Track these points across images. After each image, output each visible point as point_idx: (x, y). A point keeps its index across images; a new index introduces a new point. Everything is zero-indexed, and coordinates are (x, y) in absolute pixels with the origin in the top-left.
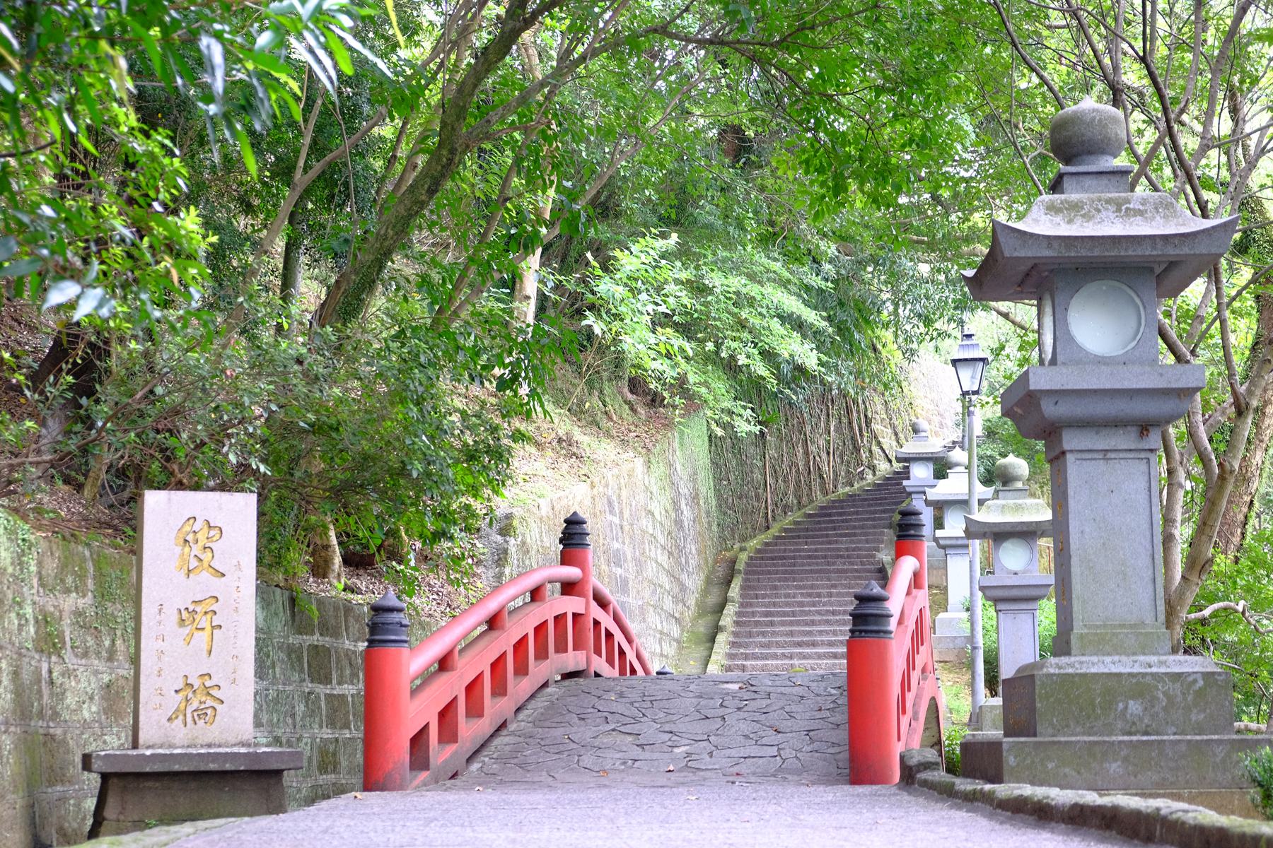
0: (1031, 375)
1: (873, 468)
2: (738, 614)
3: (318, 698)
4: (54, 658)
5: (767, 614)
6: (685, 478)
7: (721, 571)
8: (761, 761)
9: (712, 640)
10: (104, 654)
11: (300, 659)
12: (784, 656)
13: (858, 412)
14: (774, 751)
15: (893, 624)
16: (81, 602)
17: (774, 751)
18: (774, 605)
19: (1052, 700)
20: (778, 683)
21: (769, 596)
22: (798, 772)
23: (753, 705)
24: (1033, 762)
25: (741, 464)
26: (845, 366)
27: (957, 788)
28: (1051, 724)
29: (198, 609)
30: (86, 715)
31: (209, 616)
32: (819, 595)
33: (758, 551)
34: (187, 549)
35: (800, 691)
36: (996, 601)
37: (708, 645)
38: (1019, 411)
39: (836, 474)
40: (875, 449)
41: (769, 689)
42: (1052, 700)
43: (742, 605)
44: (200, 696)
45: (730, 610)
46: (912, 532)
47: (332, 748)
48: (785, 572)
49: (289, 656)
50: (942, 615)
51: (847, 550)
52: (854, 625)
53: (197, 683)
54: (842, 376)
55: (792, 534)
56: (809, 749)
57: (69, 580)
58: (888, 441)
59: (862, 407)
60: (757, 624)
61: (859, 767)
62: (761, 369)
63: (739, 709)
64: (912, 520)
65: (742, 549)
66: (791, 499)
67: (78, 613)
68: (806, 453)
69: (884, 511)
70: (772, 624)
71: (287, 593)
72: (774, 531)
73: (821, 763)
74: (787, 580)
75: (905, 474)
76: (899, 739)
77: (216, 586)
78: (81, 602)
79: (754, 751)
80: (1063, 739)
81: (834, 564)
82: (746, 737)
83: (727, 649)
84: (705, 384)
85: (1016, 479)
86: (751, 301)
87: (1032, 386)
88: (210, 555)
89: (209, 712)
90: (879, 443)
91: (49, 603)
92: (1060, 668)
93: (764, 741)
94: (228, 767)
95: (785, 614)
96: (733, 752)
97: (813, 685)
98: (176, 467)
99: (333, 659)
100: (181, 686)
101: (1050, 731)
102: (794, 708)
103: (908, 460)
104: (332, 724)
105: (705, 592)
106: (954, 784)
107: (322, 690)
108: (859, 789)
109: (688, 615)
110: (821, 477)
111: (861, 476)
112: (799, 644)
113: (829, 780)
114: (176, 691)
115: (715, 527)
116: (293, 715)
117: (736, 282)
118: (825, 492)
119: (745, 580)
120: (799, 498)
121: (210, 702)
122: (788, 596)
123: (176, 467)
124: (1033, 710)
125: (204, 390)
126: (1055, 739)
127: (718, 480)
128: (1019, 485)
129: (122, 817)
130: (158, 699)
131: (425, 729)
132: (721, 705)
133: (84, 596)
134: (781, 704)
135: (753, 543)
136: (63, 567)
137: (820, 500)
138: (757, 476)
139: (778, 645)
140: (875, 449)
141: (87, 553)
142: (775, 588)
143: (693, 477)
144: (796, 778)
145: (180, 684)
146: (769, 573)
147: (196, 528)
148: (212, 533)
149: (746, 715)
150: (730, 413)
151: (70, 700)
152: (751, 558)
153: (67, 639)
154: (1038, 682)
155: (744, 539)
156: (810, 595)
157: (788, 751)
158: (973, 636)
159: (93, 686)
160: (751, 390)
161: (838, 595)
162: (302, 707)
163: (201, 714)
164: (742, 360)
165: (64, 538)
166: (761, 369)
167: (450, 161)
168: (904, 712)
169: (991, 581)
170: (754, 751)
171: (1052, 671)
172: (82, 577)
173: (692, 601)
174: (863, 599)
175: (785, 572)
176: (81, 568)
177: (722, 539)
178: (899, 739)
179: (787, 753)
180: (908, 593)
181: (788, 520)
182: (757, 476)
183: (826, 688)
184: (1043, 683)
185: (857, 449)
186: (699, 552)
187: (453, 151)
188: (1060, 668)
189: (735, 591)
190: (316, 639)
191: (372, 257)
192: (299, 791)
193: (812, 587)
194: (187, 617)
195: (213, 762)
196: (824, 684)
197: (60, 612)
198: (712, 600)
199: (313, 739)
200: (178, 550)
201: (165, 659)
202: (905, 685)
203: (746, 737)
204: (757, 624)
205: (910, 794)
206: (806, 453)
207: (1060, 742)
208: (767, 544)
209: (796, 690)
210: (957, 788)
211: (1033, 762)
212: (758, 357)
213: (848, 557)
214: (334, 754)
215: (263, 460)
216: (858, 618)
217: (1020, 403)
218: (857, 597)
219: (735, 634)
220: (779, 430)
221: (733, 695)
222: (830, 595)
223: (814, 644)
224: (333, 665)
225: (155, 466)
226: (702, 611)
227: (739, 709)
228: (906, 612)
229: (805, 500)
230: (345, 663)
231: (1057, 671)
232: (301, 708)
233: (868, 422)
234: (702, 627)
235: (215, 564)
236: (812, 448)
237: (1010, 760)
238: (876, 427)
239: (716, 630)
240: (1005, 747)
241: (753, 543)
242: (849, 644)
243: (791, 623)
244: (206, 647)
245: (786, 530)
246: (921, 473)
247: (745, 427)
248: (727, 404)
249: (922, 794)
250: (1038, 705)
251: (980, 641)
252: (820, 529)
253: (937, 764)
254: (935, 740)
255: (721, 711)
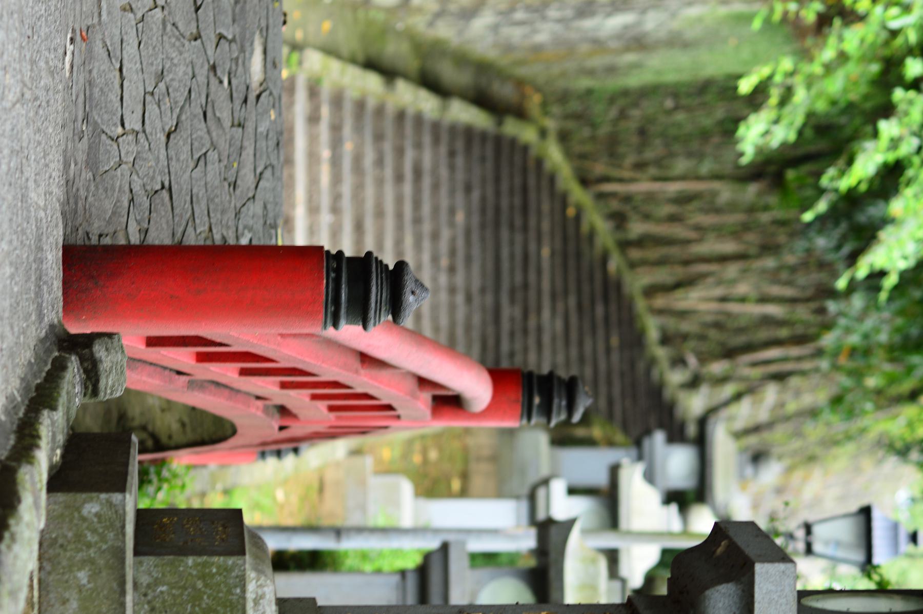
0: (781, 566)
1: (694, 383)
2: (419, 119)
5: (418, 173)
6: (675, 25)
7: (504, 91)
8: (114, 98)
9: (371, 64)
12: (336, 198)
13: (799, 359)
14: (133, 123)
15: (349, 333)
17: (133, 123)
18: (436, 187)
19: (200, 585)
20: (262, 144)
21: (452, 179)
22: (92, 162)
23: (220, 94)
24: (89, 546)
26: (881, 326)
27: (45, 412)
28: (157, 582)
32: (452, 270)
33: (539, 162)
35: (247, 179)
36: (423, 571)
37: (361, 57)
38: (720, 550)
39: (683, 314)
40: (729, 390)
41: (250, 126)
42: (200, 585)
43: (436, 127)
45: (426, 103)
46: (537, 400)
48: (497, 210)
51: (539, 329)
52: (350, 260)
54: (861, 318)
55: (572, 237)
56: (137, 188)
58: (744, 412)
59: (807, 365)
60: (400, 152)
61: (91, 265)
62: (866, 164)
63: (213, 68)
65: (543, 133)
66: (637, 228)
68: (723, 259)
69: (610, 403)
70: (399, 178)
72: (578, 195)
73: (108, 206)
74: (483, 211)
75: (676, 435)
76: (153, 342)
79: (133, 90)
80: (129, 598)
81: (512, 301)
82: (161, 75)
83: (352, 94)
84: (843, 57)
87: (760, 568)
90: (738, 397)
92: (256, 602)
93: (152, 108)
95: (417, 204)
96: (131, 49)
97: (256, 208)
101: (145, 580)
102: (214, 168)
103: (701, 443)
105: (461, 59)
106: (53, 408)
108: (53, 259)
109: (418, 23)
110: (678, 285)
111: (679, 362)
113: (72, 210)
115: (585, 83)
118: (651, 291)
119: (484, 136)
120: (641, 242)
122: (452, 211)
124: (183, 551)
126: (129, 586)
127: (675, 91)
131: (882, 274)
132: (221, 37)
134: (223, 145)
135: (554, 155)
137: (636, 282)
139: (359, 187)
140: (729, 390)
142: (468, 189)
143: (676, 41)
144: (81, 157)
146: (497, 179)
149: (201, 79)
150: (784, 100)
152: (525, 148)
154: (230, 561)
155: (564, 137)
156: (453, 253)
157: (133, 148)
158: (360, 530)
160: (830, 138)
161: (452, 308)
166: (866, 164)
168: (202, 358)
169: (458, 565)
170: (133, 90)
171: (251, 587)
173: (445, 31)
174: (397, 277)
175: (497, 210)
177: (564, 97)
178: (153, 342)
179: (128, 147)
180: (423, 382)
181: (598, 222)
182: (681, 165)
183: (250, 229)
184: (229, 570)
185: (730, 353)
186: (537, 49)
188: (256, 602)
189: (463, 113)
193: (468, 259)
196: (259, 226)
198: (448, 73)
202: (252, 363)
203: (161, 75)
204: (400, 152)
205: (42, 341)
206: (723, 259)
207: (123, 593)
208: (552, 179)
209: (247, 179)
210: (45, 412)
211: (89, 546)
212: (891, 157)
213: (525, 331)
216: (362, 268)
217: (734, 550)
218: (401, 266)
219: (380, 111)
220: (766, 208)
221: (241, 60)
222: (452, 290)
226: (429, 50)
227: (213, 68)
228: (385, 374)
229: (635, 254)
231: (250, 596)
233: (780, 377)
234: (395, 50)
236: (732, 270)
237: (92, 506)
238: (771, 393)
239: (389, 74)
240: (116, 497)
241: (554, 155)
242: (317, 251)
243: (399, 216)
245: (578, 218)
246: (678, 463)
247: (757, 134)
248: (800, 96)
249: (40, 359)
250: (190, 561)
251: (348, 545)
252: (579, 282)
253: (95, 393)
254: (164, 439)
255: (209, 36)
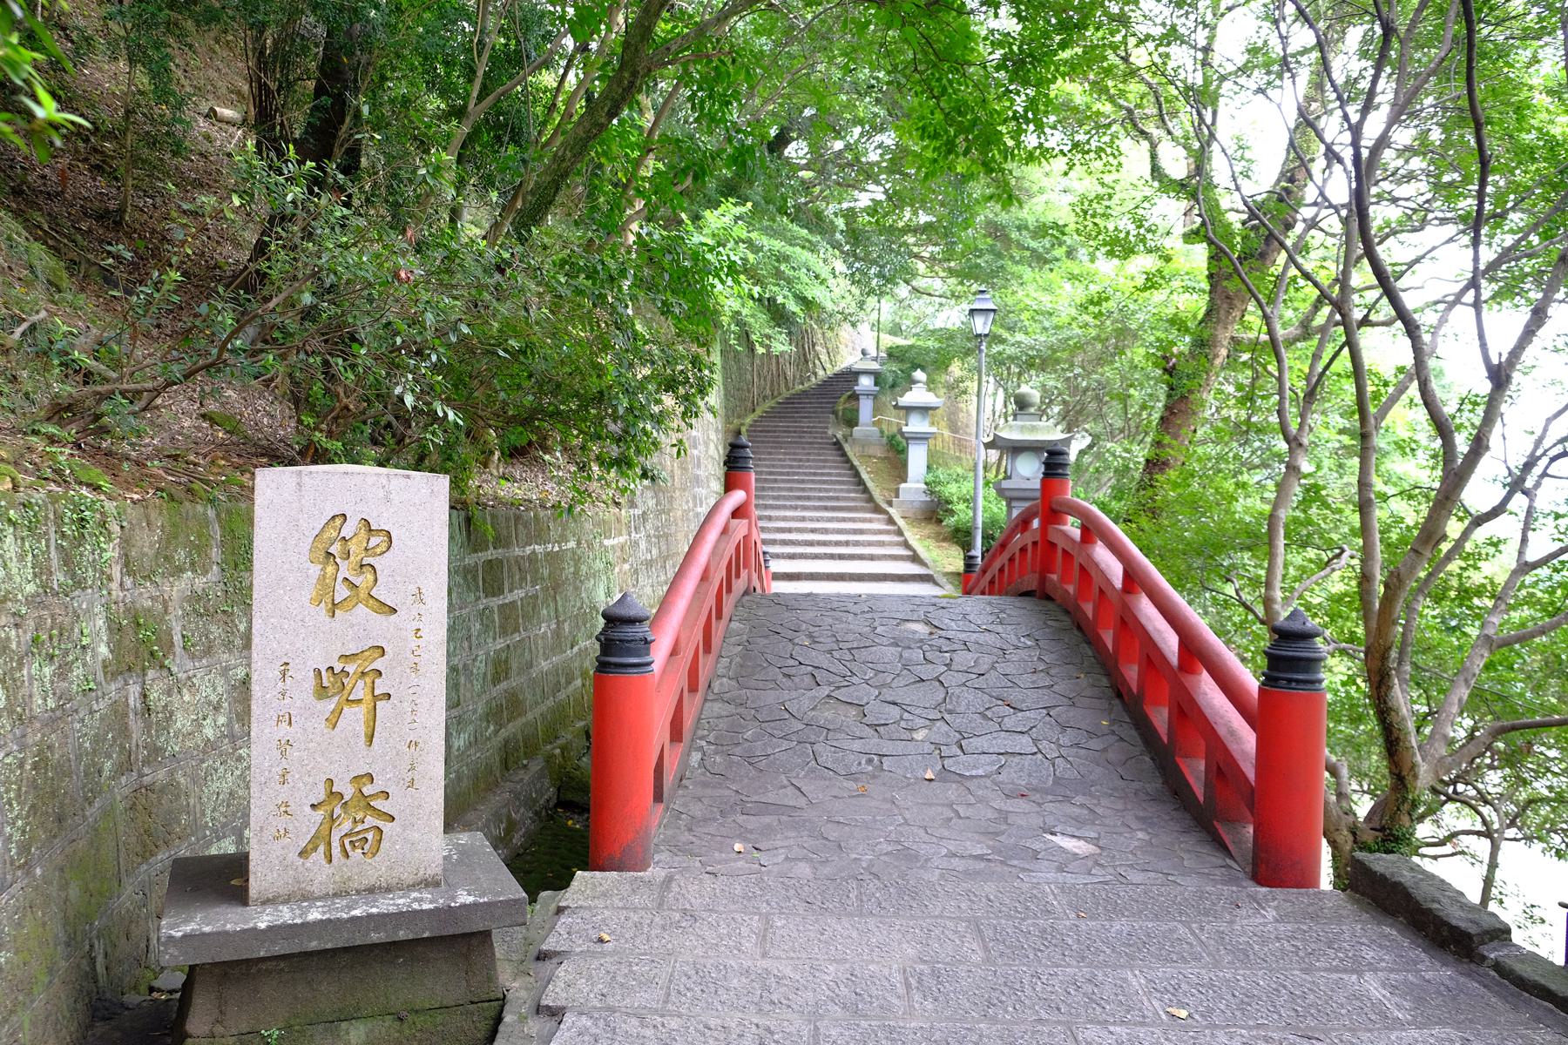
1: (815, 374)
3: (492, 612)
4: (151, 674)
10: (238, 642)
11: (475, 578)
16: (200, 583)
25: (739, 368)
29: (351, 668)
30: (209, 732)
31: (368, 680)
34: (330, 569)
44: (353, 809)
47: (504, 656)
49: (465, 578)
50: (903, 485)
53: (348, 792)
55: (771, 415)
57: (181, 555)
64: (1060, 459)
66: (768, 392)
67: (195, 598)
71: (463, 513)
72: (759, 412)
77: (379, 628)
78: (200, 583)
85: (1031, 405)
86: (786, 258)
88: (370, 577)
89: (370, 836)
91: (144, 597)
94: (402, 935)
98: (341, 390)
99: (505, 569)
100: (322, 797)
104: (504, 632)
107: (495, 602)
112: (799, 498)
114: (313, 806)
116: (469, 638)
117: (777, 245)
121: (370, 821)
123: (341, 390)
125: (370, 300)
128: (1032, 410)
129: (219, 1029)
130: (282, 822)
133: (205, 573)
135: (748, 420)
136: (169, 539)
137: (786, 394)
138: (749, 377)
141: (211, 513)
145: (320, 794)
147: (347, 531)
148: (374, 541)
151: (182, 722)
153: (177, 638)
159: (220, 689)
162: (478, 626)
163: (356, 840)
164: (780, 300)
165: (172, 498)
167: (632, 84)
172: (201, 548)
176: (199, 536)
185: (806, 361)
187: (634, 74)
190: (491, 554)
191: (549, 179)
192: (475, 711)
194: (331, 684)
195: (376, 930)
197: (165, 604)
199: (487, 654)
200: (315, 570)
201: (294, 754)
214: (506, 661)
215: (448, 401)
223: (809, 498)
224: (505, 575)
225: (317, 388)
230: (515, 569)
232: (476, 627)
235: (380, 593)
244: (361, 729)
